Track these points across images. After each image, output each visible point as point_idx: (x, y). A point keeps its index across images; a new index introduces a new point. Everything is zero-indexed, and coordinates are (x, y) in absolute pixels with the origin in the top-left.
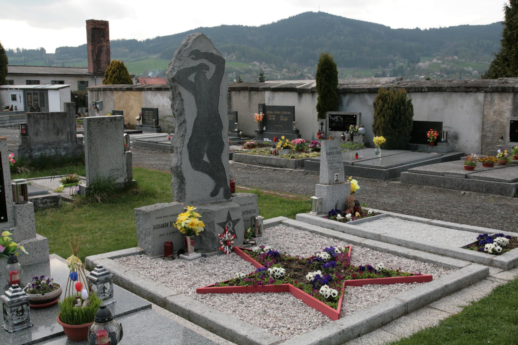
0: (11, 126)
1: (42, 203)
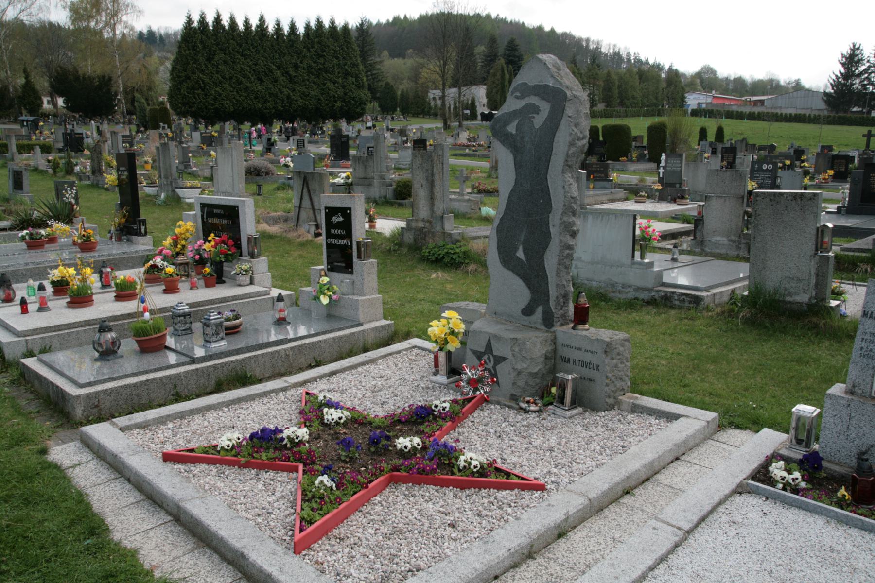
1: (679, 300)
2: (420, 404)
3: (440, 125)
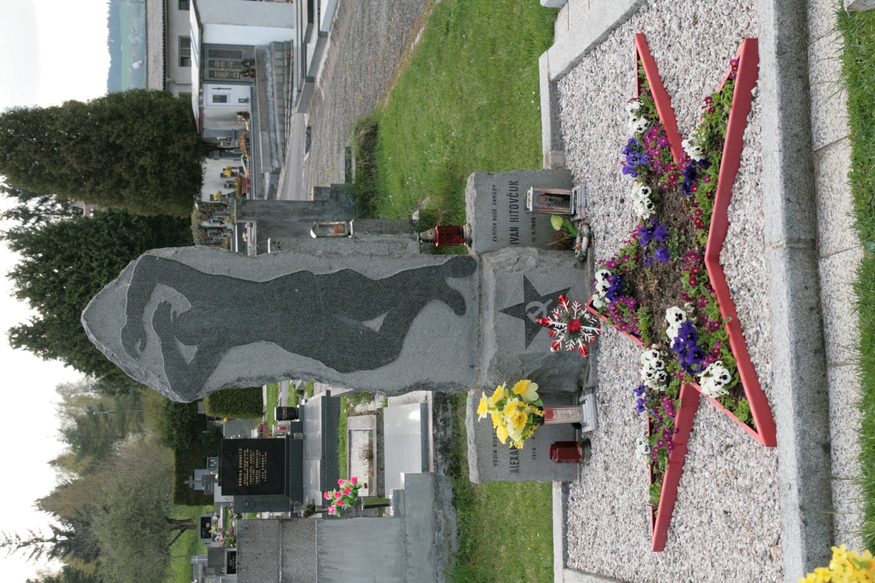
0: (283, 131)
1: (444, 428)
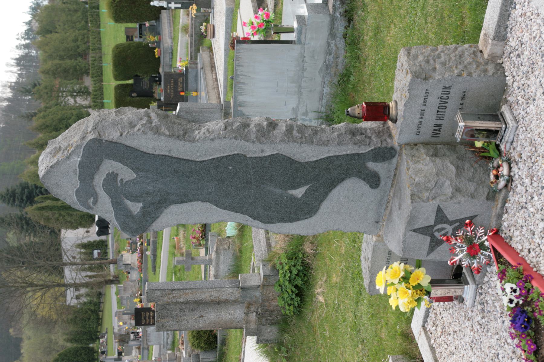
2: (508, 323)
3: (113, 289)
